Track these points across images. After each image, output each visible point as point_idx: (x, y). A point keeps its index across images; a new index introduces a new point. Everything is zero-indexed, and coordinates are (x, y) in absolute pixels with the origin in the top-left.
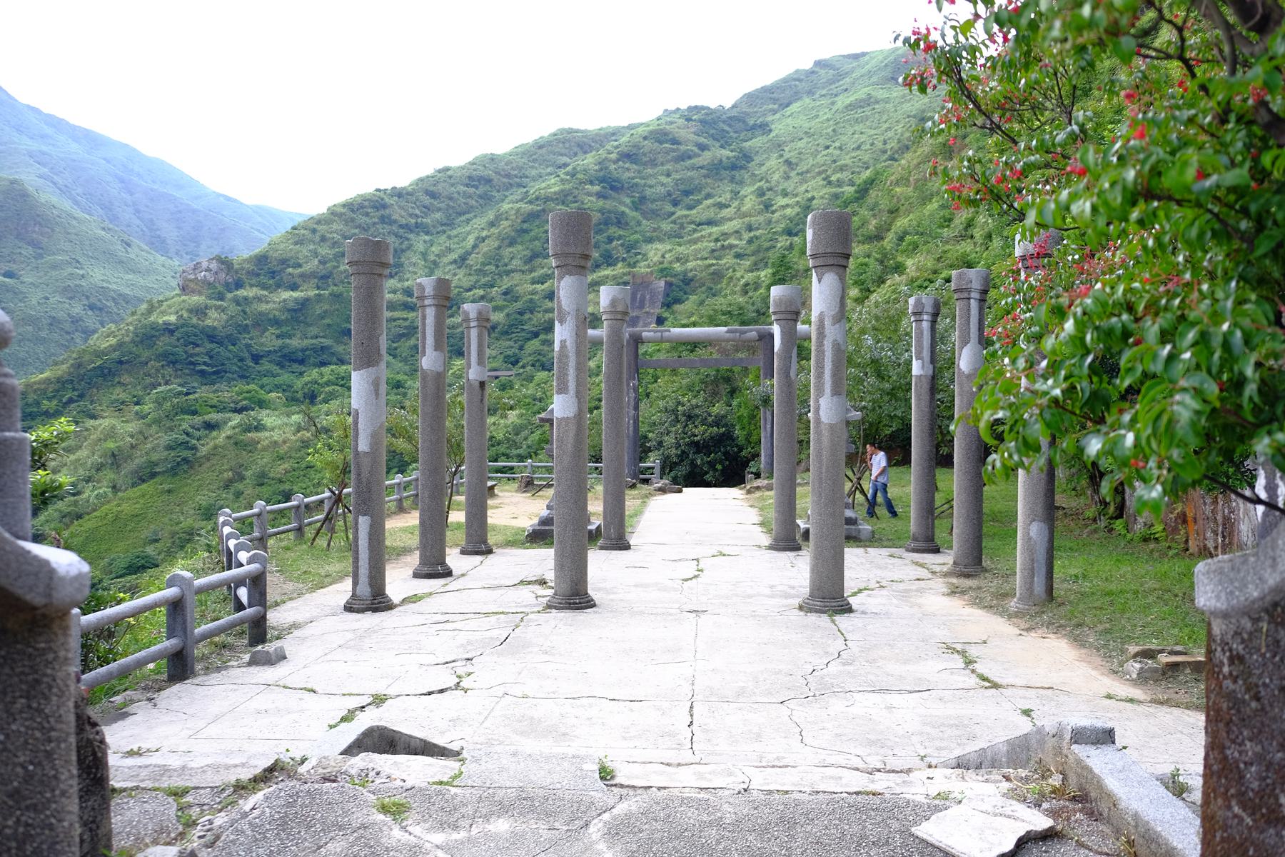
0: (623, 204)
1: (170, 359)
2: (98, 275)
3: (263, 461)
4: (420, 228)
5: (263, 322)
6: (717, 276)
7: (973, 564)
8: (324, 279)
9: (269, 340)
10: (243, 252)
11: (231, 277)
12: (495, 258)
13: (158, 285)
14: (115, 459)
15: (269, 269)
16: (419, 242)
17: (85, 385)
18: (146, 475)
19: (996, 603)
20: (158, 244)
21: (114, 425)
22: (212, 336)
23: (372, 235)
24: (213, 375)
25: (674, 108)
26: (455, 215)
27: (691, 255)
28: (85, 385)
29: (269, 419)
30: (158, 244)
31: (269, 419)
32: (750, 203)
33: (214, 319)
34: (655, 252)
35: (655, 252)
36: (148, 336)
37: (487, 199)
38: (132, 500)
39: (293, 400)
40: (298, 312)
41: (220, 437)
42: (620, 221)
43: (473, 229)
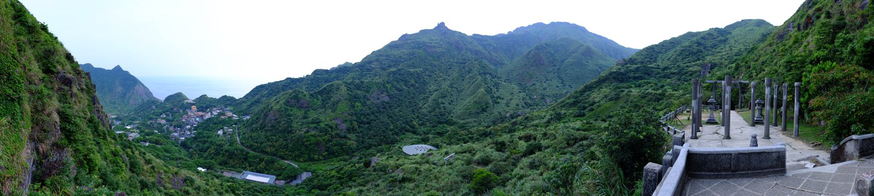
0: (702, 48)
1: (614, 78)
2: (601, 62)
3: (632, 98)
4: (660, 52)
5: (631, 71)
6: (721, 64)
7: (785, 129)
8: (642, 63)
9: (632, 75)
10: (627, 58)
11: (626, 62)
12: (675, 59)
13: (612, 64)
14: (606, 96)
15: (632, 61)
16: (660, 55)
17: (601, 82)
18: (611, 100)
19: (790, 136)
20: (611, 56)
21: (605, 90)
22: (622, 74)
23: (652, 52)
24: (622, 81)
25: (218, 96)
26: (667, 50)
27: (716, 59)
28: (711, 104)
29: (633, 90)
30: (611, 56)
31: (633, 90)
32: (728, 49)
33: (622, 71)
34: (708, 58)
35: (708, 58)
36: (611, 74)
37: (673, 47)
38: (609, 104)
39: (636, 87)
40: (637, 69)
41: (624, 93)
42: (701, 52)
43: (671, 53)
